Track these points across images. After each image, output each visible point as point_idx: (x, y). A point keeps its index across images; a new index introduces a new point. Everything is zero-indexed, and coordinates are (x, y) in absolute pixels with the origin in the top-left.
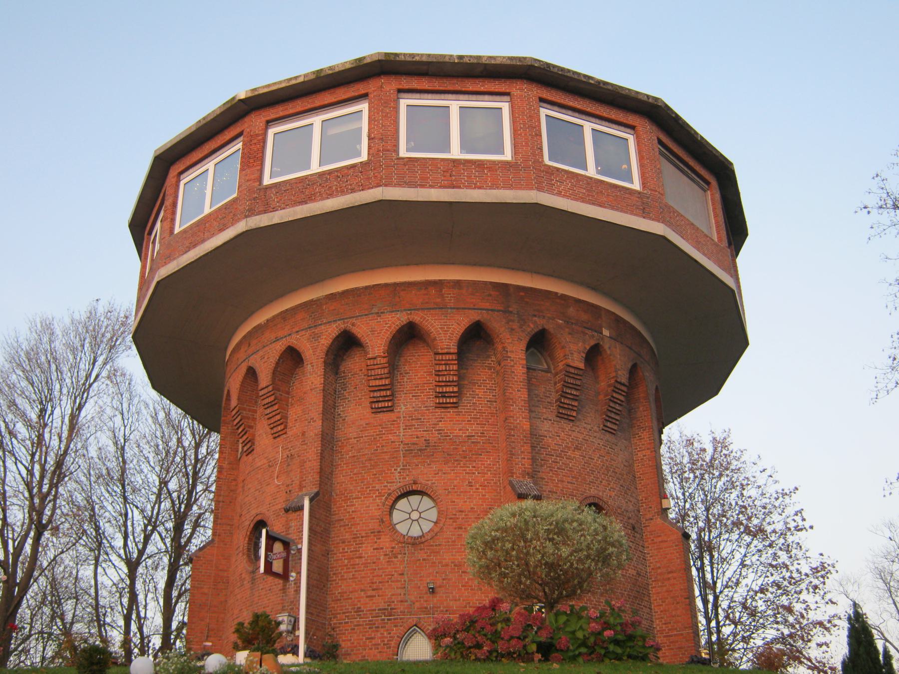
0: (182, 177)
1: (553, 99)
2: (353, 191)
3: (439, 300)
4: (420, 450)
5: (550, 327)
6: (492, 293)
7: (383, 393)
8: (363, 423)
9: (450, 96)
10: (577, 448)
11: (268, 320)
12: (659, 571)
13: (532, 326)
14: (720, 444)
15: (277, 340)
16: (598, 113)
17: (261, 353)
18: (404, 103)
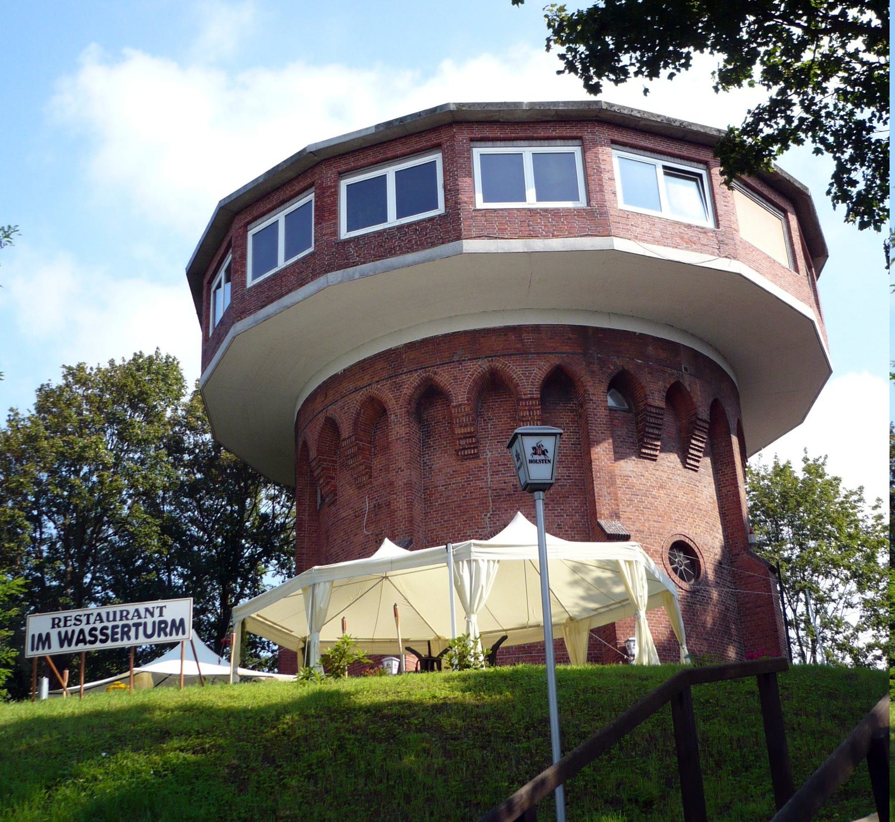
0: (249, 227)
1: (625, 140)
2: (433, 245)
3: (519, 346)
4: (509, 495)
5: (630, 367)
6: (571, 336)
7: (469, 441)
8: (450, 470)
9: (522, 143)
10: (661, 487)
11: (344, 370)
12: (748, 606)
13: (612, 368)
14: (814, 469)
15: (357, 390)
16: (669, 150)
17: (340, 403)
18: (477, 152)
